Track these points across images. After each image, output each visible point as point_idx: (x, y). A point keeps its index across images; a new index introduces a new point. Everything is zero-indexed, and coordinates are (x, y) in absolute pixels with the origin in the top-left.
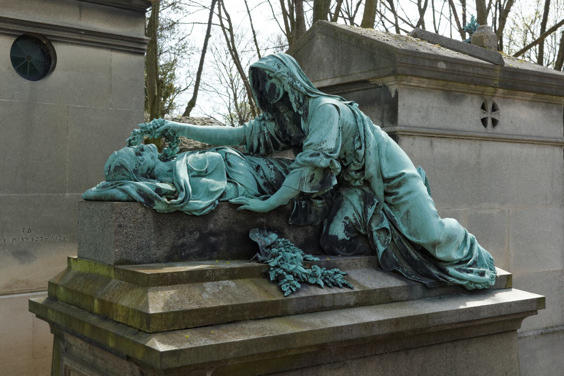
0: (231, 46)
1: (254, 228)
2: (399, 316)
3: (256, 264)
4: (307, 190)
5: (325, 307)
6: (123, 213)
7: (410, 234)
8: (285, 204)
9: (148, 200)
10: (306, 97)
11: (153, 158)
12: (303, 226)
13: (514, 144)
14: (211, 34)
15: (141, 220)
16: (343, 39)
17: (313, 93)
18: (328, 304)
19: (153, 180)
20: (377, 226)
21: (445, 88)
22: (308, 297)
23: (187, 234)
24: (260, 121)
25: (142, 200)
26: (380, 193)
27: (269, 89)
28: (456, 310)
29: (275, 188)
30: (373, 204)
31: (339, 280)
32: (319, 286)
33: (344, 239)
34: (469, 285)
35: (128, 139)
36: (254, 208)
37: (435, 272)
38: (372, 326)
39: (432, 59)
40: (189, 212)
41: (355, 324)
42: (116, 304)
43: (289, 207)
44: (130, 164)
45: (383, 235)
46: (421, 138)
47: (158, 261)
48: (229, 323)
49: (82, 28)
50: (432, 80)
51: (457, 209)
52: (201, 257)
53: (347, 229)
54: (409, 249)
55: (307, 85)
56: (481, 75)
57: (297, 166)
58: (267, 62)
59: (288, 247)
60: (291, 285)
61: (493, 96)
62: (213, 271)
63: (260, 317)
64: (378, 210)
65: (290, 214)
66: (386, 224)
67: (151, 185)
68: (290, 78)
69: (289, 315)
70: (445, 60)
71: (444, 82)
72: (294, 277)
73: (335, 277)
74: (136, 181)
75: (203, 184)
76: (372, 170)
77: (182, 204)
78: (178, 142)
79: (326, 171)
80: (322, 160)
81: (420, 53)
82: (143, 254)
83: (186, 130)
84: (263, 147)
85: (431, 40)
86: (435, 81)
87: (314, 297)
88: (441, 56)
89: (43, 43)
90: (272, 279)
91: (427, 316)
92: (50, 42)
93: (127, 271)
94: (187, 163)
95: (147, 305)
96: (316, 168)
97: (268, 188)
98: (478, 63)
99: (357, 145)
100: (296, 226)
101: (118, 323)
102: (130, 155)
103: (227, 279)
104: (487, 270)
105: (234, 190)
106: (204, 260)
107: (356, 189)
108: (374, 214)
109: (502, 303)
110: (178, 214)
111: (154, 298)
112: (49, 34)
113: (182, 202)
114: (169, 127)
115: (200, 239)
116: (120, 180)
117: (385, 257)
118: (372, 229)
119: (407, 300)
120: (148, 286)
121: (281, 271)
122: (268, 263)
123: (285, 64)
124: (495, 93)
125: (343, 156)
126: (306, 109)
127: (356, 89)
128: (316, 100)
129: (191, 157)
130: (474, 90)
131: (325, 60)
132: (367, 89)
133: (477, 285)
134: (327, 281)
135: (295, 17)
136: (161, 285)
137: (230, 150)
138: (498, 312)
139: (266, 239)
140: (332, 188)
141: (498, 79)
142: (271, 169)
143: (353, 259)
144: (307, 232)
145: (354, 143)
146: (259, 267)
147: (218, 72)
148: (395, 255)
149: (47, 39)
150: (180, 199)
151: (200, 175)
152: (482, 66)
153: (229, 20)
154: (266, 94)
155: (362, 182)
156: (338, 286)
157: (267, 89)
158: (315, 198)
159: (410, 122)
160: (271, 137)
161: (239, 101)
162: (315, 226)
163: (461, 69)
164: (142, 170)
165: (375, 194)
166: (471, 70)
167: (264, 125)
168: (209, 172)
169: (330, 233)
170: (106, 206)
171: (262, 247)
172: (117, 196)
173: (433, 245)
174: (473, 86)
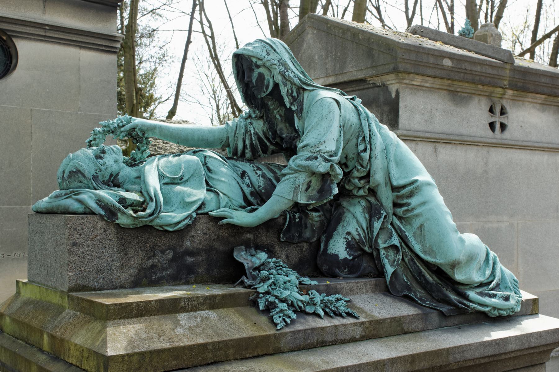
0: (213, 53)
1: (239, 245)
2: (415, 352)
3: (242, 290)
4: (302, 200)
5: (326, 342)
6: (78, 228)
7: (425, 252)
8: (276, 217)
9: (110, 213)
10: (301, 90)
11: (116, 161)
12: (297, 243)
13: (523, 151)
14: (191, 40)
15: (101, 237)
16: (337, 34)
17: (308, 85)
18: (329, 338)
19: (117, 189)
20: (385, 242)
21: (450, 89)
22: (305, 330)
23: (158, 254)
24: (246, 119)
25: (102, 213)
26: (388, 203)
27: (257, 81)
28: (480, 343)
29: (264, 198)
30: (380, 217)
31: (342, 308)
32: (319, 316)
33: (345, 259)
34: (492, 311)
35: (88, 140)
36: (239, 222)
37: (453, 297)
38: (384, 365)
39: (437, 56)
40: (160, 226)
41: (363, 364)
42: (68, 341)
43: (281, 220)
44: (88, 169)
45: (391, 253)
46: (424, 143)
47: (122, 287)
48: (208, 364)
49: (47, 23)
50: (436, 79)
51: (463, 223)
52: (176, 280)
53: (349, 246)
54: (423, 270)
55: (301, 76)
56: (489, 74)
57: (291, 172)
58: (254, 48)
59: (281, 269)
60: (284, 315)
61: (501, 98)
62: (189, 299)
63: (248, 356)
64: (386, 224)
65: (282, 229)
66: (395, 241)
67: (114, 194)
68: (281, 67)
69: (283, 352)
70: (451, 56)
71: (450, 82)
72: (288, 305)
73: (337, 305)
74: (96, 189)
75: (178, 194)
76: (378, 177)
77: (151, 218)
78: (148, 143)
79: (325, 177)
80: (320, 164)
81: (423, 48)
82: (104, 279)
83: (158, 129)
84: (249, 149)
85: (432, 37)
86: (440, 80)
87: (313, 329)
88: (447, 52)
89: (3, 39)
90: (261, 308)
91: (448, 350)
92: (10, 37)
93: (83, 300)
94: (158, 168)
95: (104, 344)
96: (314, 174)
97: (260, 197)
98: (487, 61)
99: (361, 147)
100: (289, 242)
101: (71, 364)
102: (88, 158)
103: (207, 309)
104: (512, 294)
105: (214, 201)
106: (179, 285)
107: (359, 199)
108: (381, 229)
109: (531, 333)
110: (147, 229)
111: (115, 335)
112: (9, 28)
113: (152, 214)
114: (137, 126)
115: (174, 259)
116: (77, 188)
117: (394, 280)
118: (379, 246)
119: (421, 331)
120: (107, 320)
121: (272, 299)
122: (256, 288)
123: (275, 50)
124: (504, 94)
125: (344, 161)
126: (301, 105)
127: (352, 89)
128: (312, 93)
129: (163, 160)
130: (481, 91)
131: (316, 58)
132: (363, 89)
133: (501, 312)
134: (327, 310)
135: (279, 25)
136: (124, 318)
137: (209, 153)
138: (527, 344)
139: (254, 259)
140: (332, 198)
141: (508, 79)
142: (259, 176)
143: (357, 283)
144: (301, 250)
145: (357, 145)
146: (246, 293)
147: (201, 82)
148: (406, 277)
149: (6, 34)
150: (148, 211)
151: (174, 182)
152: (491, 65)
153: (210, 27)
154: (253, 87)
155: (367, 191)
156: (340, 315)
157: (254, 81)
158: (311, 210)
159: (413, 125)
160: (259, 138)
161: (222, 112)
162: (311, 243)
163: (469, 67)
164: (103, 176)
165: (382, 205)
166: (478, 68)
167: (251, 124)
168: (185, 179)
169: (329, 252)
170: (57, 220)
171: (249, 268)
172: (71, 207)
173: (452, 265)
174: (480, 87)
